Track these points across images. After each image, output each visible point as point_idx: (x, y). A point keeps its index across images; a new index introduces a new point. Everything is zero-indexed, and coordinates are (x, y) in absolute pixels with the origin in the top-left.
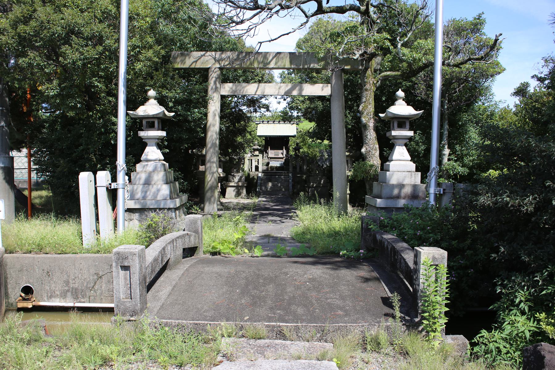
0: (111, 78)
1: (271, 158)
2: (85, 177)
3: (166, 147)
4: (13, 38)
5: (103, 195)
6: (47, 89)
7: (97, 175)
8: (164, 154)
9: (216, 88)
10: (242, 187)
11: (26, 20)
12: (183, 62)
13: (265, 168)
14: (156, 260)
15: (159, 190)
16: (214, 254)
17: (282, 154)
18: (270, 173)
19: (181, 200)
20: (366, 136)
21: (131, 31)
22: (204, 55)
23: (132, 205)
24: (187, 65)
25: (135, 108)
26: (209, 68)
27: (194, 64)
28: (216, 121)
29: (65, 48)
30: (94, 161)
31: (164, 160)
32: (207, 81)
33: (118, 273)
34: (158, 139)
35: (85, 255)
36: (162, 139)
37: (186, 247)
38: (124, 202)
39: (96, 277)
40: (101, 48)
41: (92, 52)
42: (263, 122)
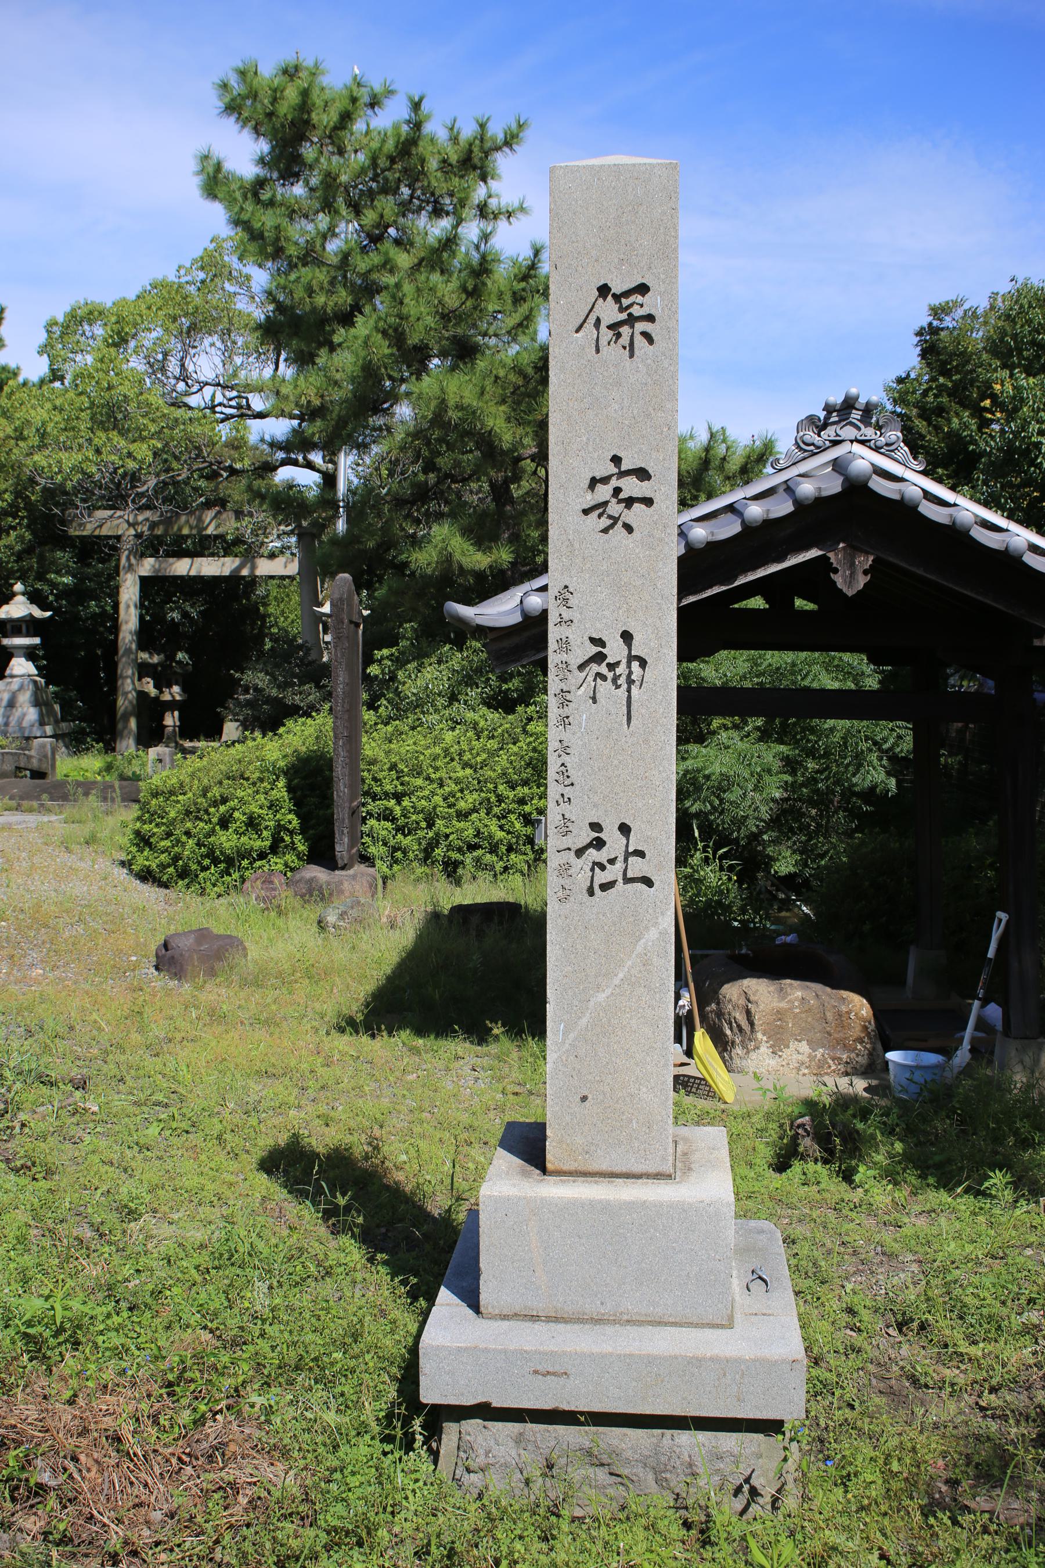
8: (37, 667)
9: (130, 566)
15: (24, 715)
22: (111, 517)
36: (34, 647)
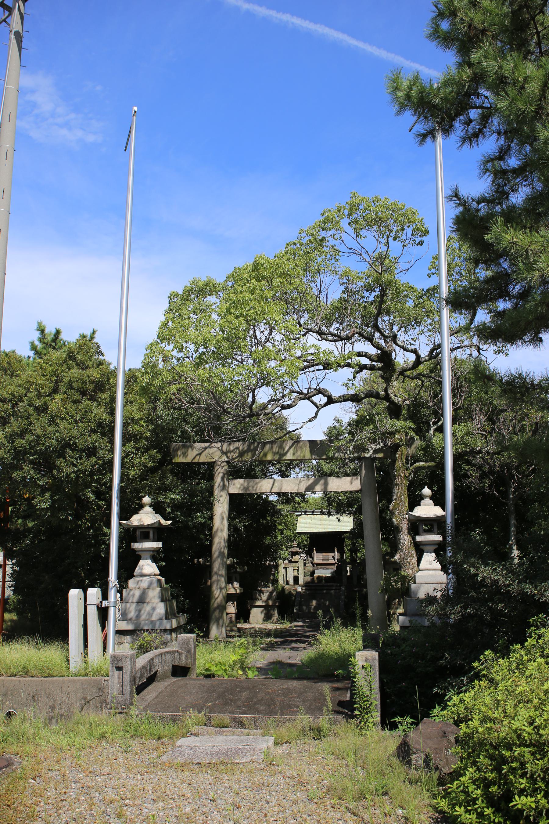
0: (104, 494)
1: (317, 564)
2: (74, 594)
3: (162, 560)
4: (9, 452)
5: (92, 612)
6: (39, 502)
7: (88, 593)
8: (159, 568)
10: (273, 607)
11: (22, 434)
12: (185, 455)
13: (309, 578)
14: (144, 667)
15: (154, 609)
16: (208, 676)
17: (334, 558)
18: (315, 587)
19: (178, 622)
20: (399, 540)
21: (127, 438)
23: (124, 626)
24: (189, 460)
25: (128, 519)
26: (214, 462)
27: (198, 457)
28: (224, 526)
29: (59, 462)
30: (81, 577)
31: (159, 575)
32: (213, 479)
33: (114, 672)
34: (153, 551)
35: (72, 678)
36: (157, 551)
37: (176, 664)
38: (115, 622)
39: (83, 702)
40: (94, 459)
41: (87, 464)
42: (306, 512)
